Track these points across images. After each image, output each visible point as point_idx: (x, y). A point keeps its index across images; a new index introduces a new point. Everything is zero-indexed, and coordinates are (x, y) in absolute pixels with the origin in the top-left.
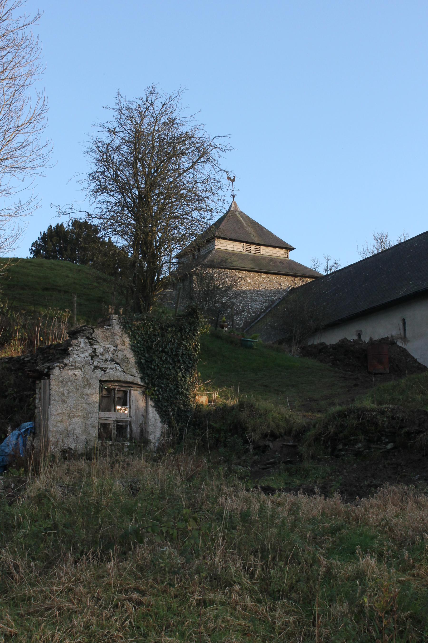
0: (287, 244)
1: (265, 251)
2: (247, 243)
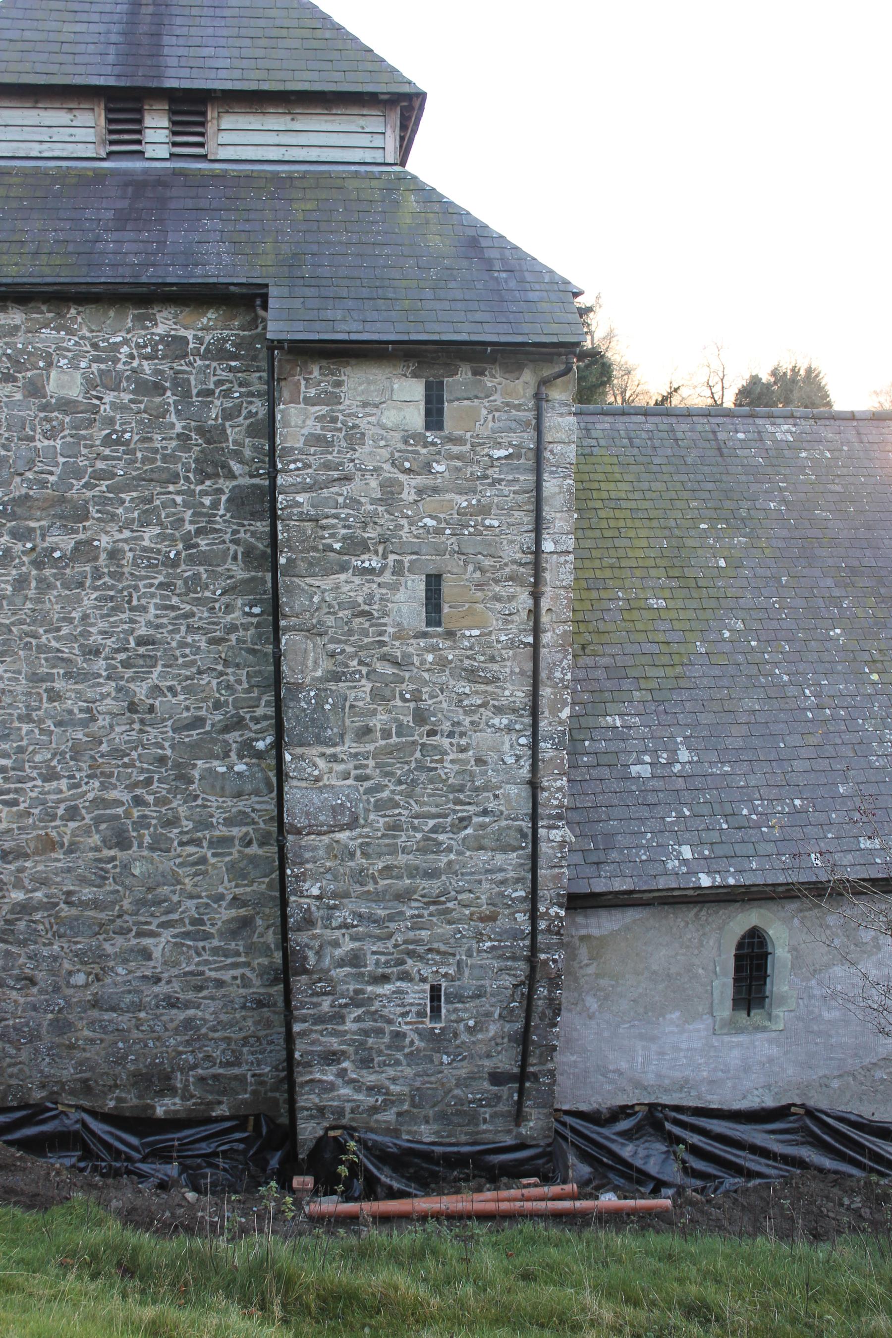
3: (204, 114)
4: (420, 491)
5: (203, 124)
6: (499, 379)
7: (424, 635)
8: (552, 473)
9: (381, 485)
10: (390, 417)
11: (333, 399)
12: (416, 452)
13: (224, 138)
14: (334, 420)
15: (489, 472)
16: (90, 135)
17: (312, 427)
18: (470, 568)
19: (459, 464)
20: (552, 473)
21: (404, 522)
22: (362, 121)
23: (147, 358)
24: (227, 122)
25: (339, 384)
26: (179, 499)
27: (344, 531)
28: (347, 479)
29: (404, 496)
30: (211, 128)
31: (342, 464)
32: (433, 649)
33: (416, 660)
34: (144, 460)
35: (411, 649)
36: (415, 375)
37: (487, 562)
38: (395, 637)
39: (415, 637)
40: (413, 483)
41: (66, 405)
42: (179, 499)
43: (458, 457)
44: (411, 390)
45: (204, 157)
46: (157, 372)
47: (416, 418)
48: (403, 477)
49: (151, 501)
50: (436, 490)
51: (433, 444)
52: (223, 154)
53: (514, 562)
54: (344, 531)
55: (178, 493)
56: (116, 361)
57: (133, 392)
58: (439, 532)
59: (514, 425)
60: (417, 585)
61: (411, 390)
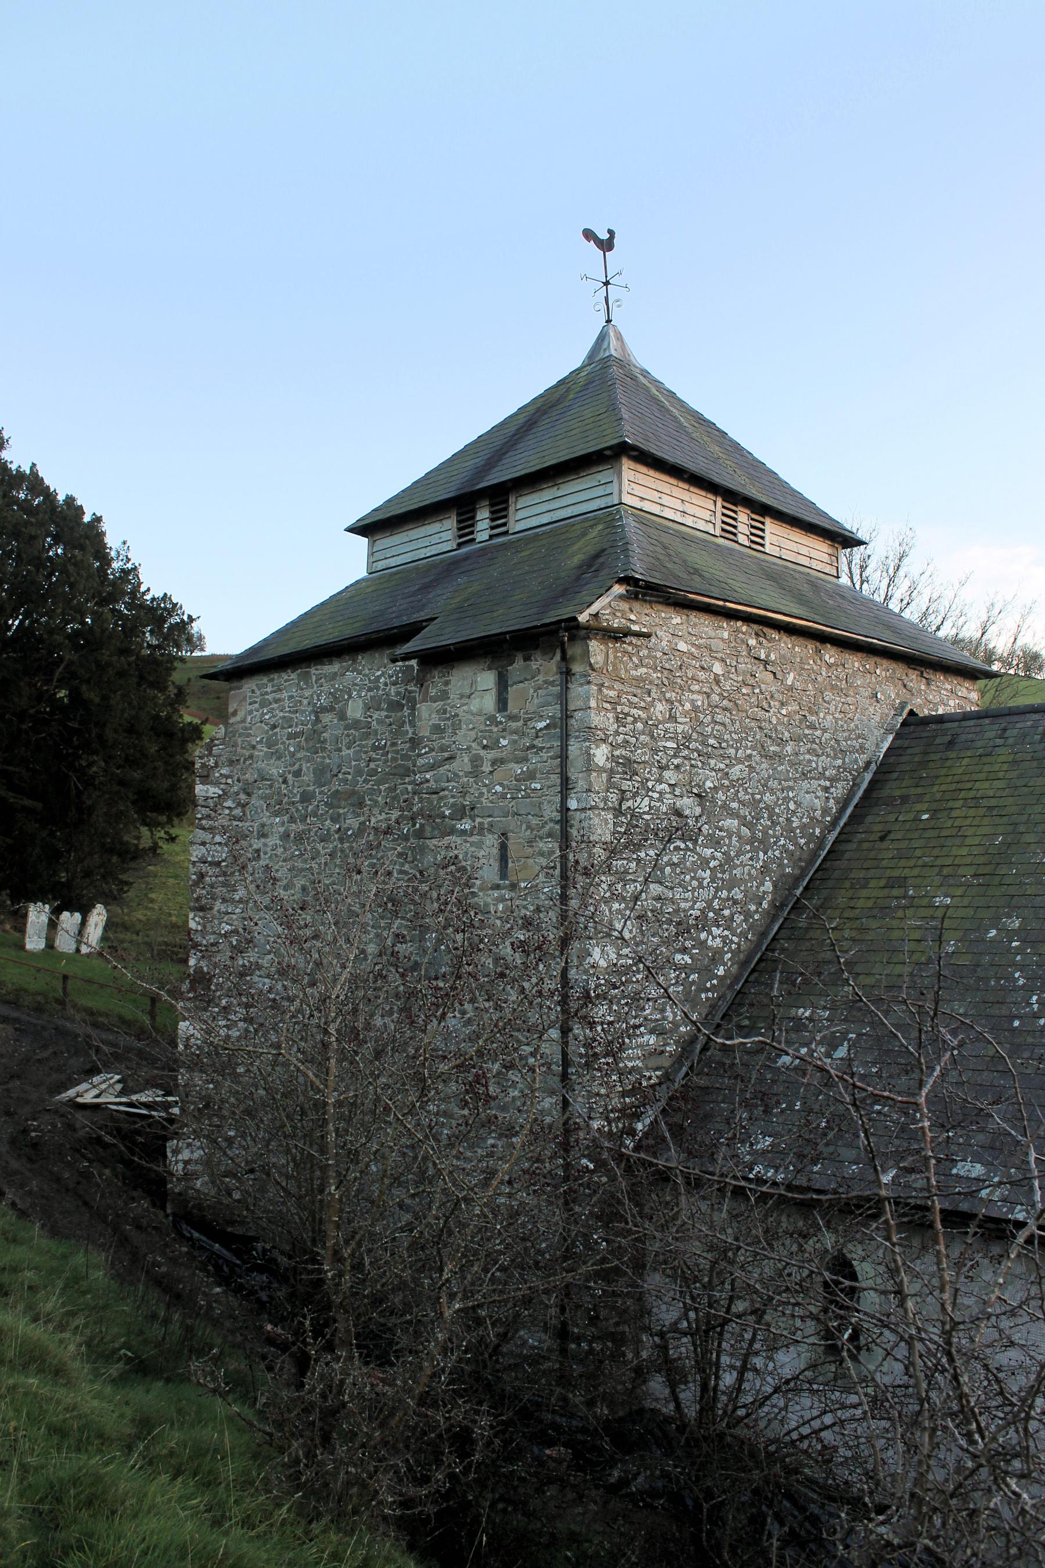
0: (825, 515)
1: (775, 534)
2: (732, 497)
3: (507, 501)
4: (494, 763)
5: (506, 509)
6: (540, 662)
7: (497, 887)
8: (577, 737)
9: (471, 761)
10: (474, 705)
11: (444, 696)
12: (491, 731)
13: (521, 514)
14: (445, 712)
15: (535, 742)
16: (448, 535)
17: (435, 719)
18: (524, 827)
19: (516, 737)
20: (577, 737)
21: (485, 790)
22: (599, 476)
23: (394, 684)
24: (522, 502)
25: (447, 683)
26: (410, 788)
27: (452, 800)
28: (452, 758)
29: (484, 769)
30: (511, 509)
31: (449, 746)
32: (502, 899)
33: (492, 909)
34: (394, 759)
35: (489, 900)
36: (490, 669)
37: (535, 821)
38: (481, 889)
39: (492, 888)
40: (489, 756)
41: (356, 724)
42: (410, 788)
43: (515, 732)
44: (487, 679)
45: (506, 533)
46: (398, 693)
47: (488, 702)
48: (482, 753)
49: (395, 789)
50: (502, 761)
51: (501, 723)
52: (519, 527)
53: (551, 820)
54: (452, 800)
55: (410, 783)
56: (378, 688)
57: (387, 710)
58: (503, 796)
59: (550, 699)
60: (491, 841)
61: (487, 679)
